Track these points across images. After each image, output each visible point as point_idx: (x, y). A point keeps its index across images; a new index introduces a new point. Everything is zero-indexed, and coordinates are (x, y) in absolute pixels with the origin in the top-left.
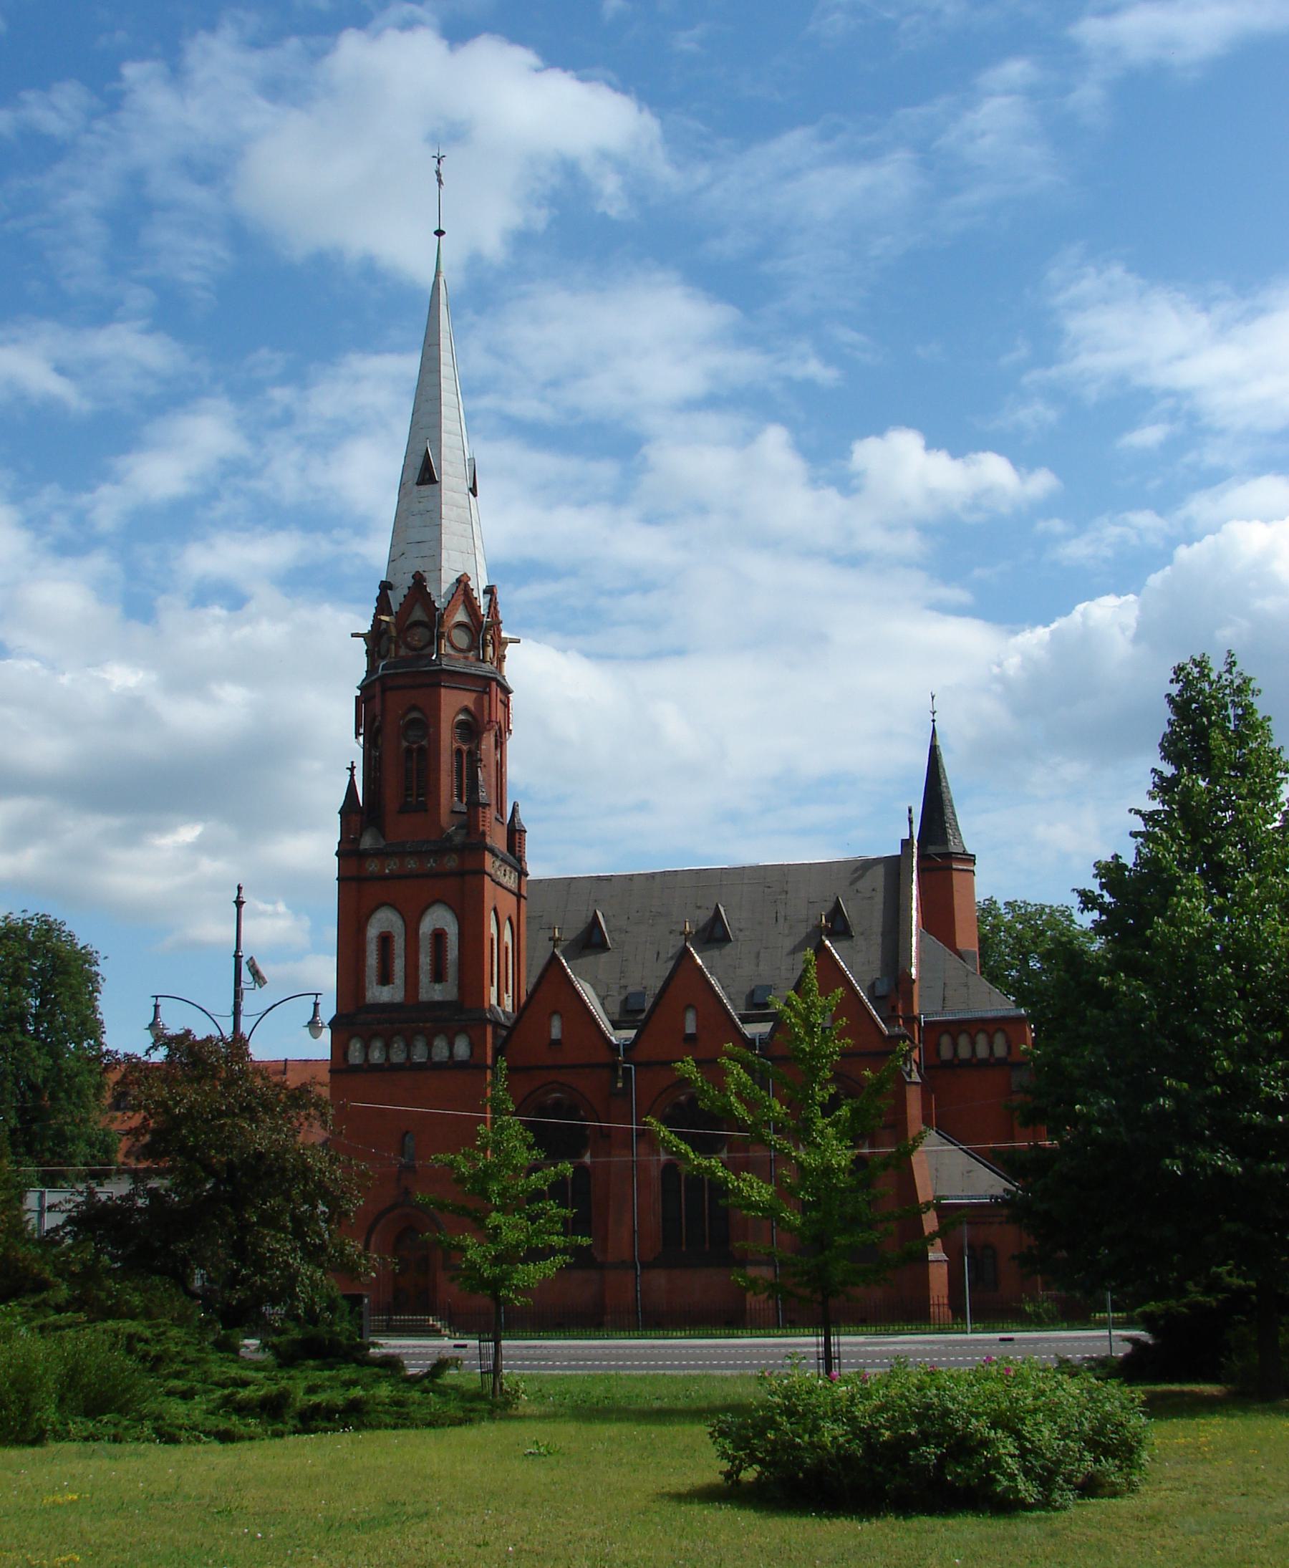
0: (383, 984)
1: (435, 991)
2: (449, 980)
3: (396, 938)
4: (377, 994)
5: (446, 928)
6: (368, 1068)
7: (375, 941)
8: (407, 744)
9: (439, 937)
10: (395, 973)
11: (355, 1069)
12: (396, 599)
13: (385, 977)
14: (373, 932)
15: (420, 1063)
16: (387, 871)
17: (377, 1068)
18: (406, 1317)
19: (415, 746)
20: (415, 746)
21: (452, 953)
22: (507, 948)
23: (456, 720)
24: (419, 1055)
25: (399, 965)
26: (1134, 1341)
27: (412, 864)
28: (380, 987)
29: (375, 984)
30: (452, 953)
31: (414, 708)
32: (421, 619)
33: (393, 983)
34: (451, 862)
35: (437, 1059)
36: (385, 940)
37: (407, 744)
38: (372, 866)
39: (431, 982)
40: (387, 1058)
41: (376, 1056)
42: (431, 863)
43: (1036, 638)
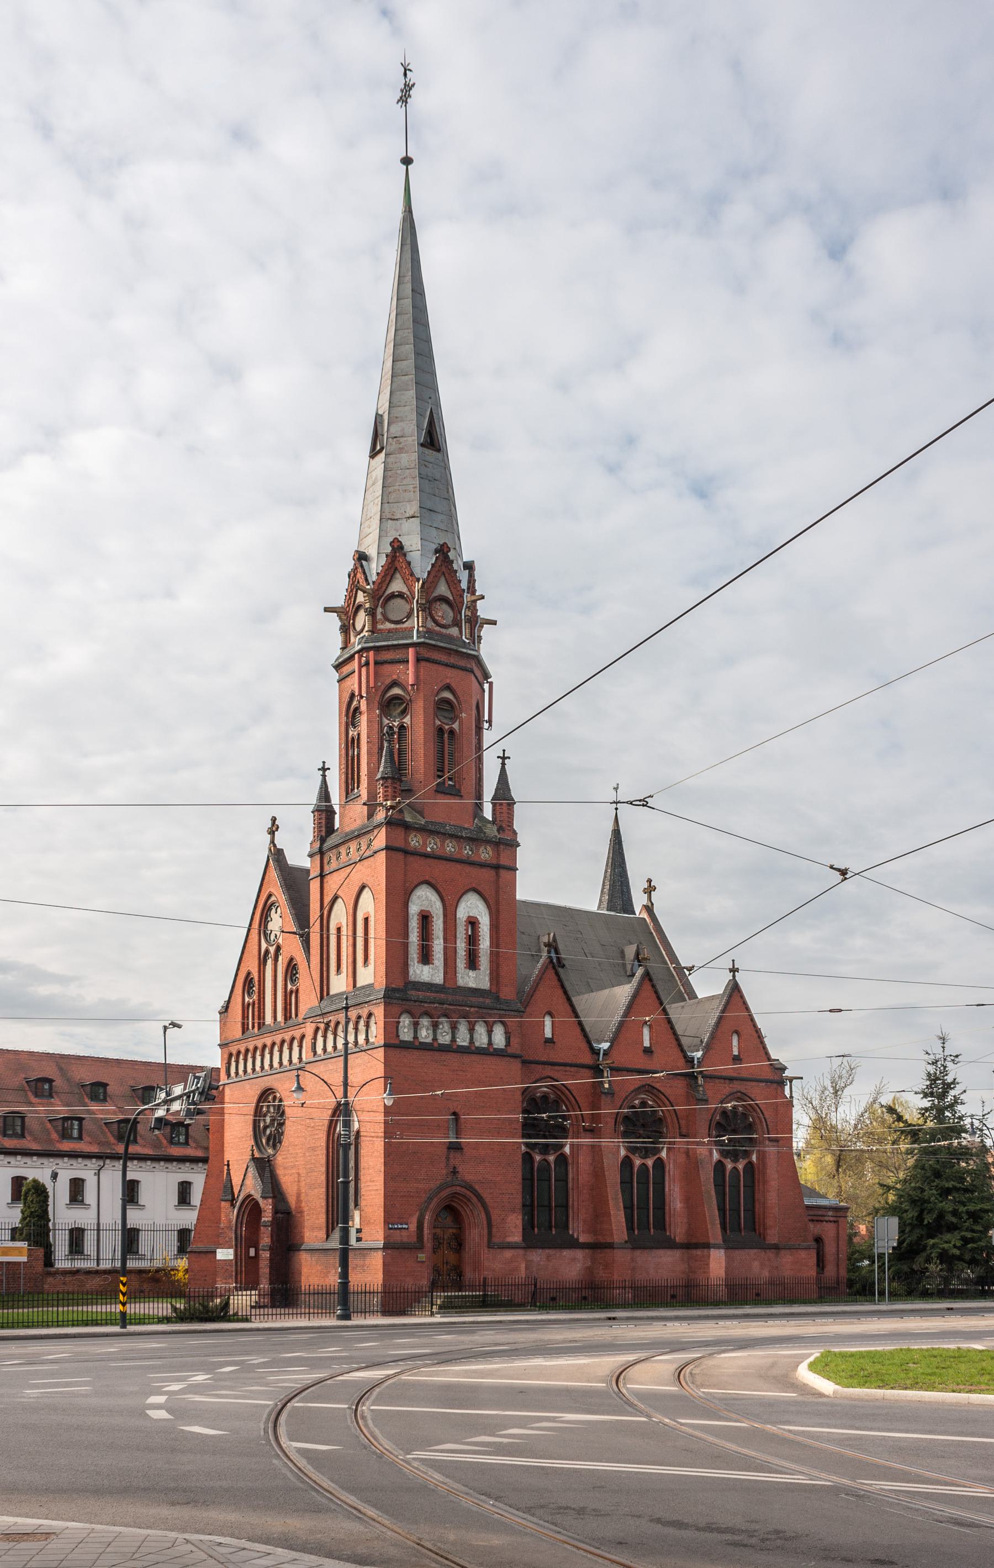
0: (425, 964)
1: (469, 977)
2: (482, 968)
3: (434, 919)
4: (418, 972)
5: (478, 917)
6: (415, 1046)
7: (416, 918)
8: (440, 723)
9: (473, 923)
10: (434, 953)
11: (405, 1046)
12: (375, 567)
13: (426, 958)
14: (414, 909)
15: (462, 1046)
16: (429, 849)
17: (425, 1047)
18: (453, 1294)
19: (447, 727)
20: (447, 727)
21: (485, 944)
22: (339, 930)
23: (385, 699)
24: (463, 1039)
25: (438, 946)
26: (821, 1352)
27: (450, 847)
28: (420, 965)
29: (416, 962)
30: (485, 944)
31: (448, 687)
32: (445, 594)
33: (433, 964)
34: (485, 854)
35: (477, 1044)
36: (425, 918)
37: (440, 723)
38: (415, 841)
39: (465, 968)
40: (435, 1039)
41: (425, 1035)
42: (467, 851)
43: (439, 697)
